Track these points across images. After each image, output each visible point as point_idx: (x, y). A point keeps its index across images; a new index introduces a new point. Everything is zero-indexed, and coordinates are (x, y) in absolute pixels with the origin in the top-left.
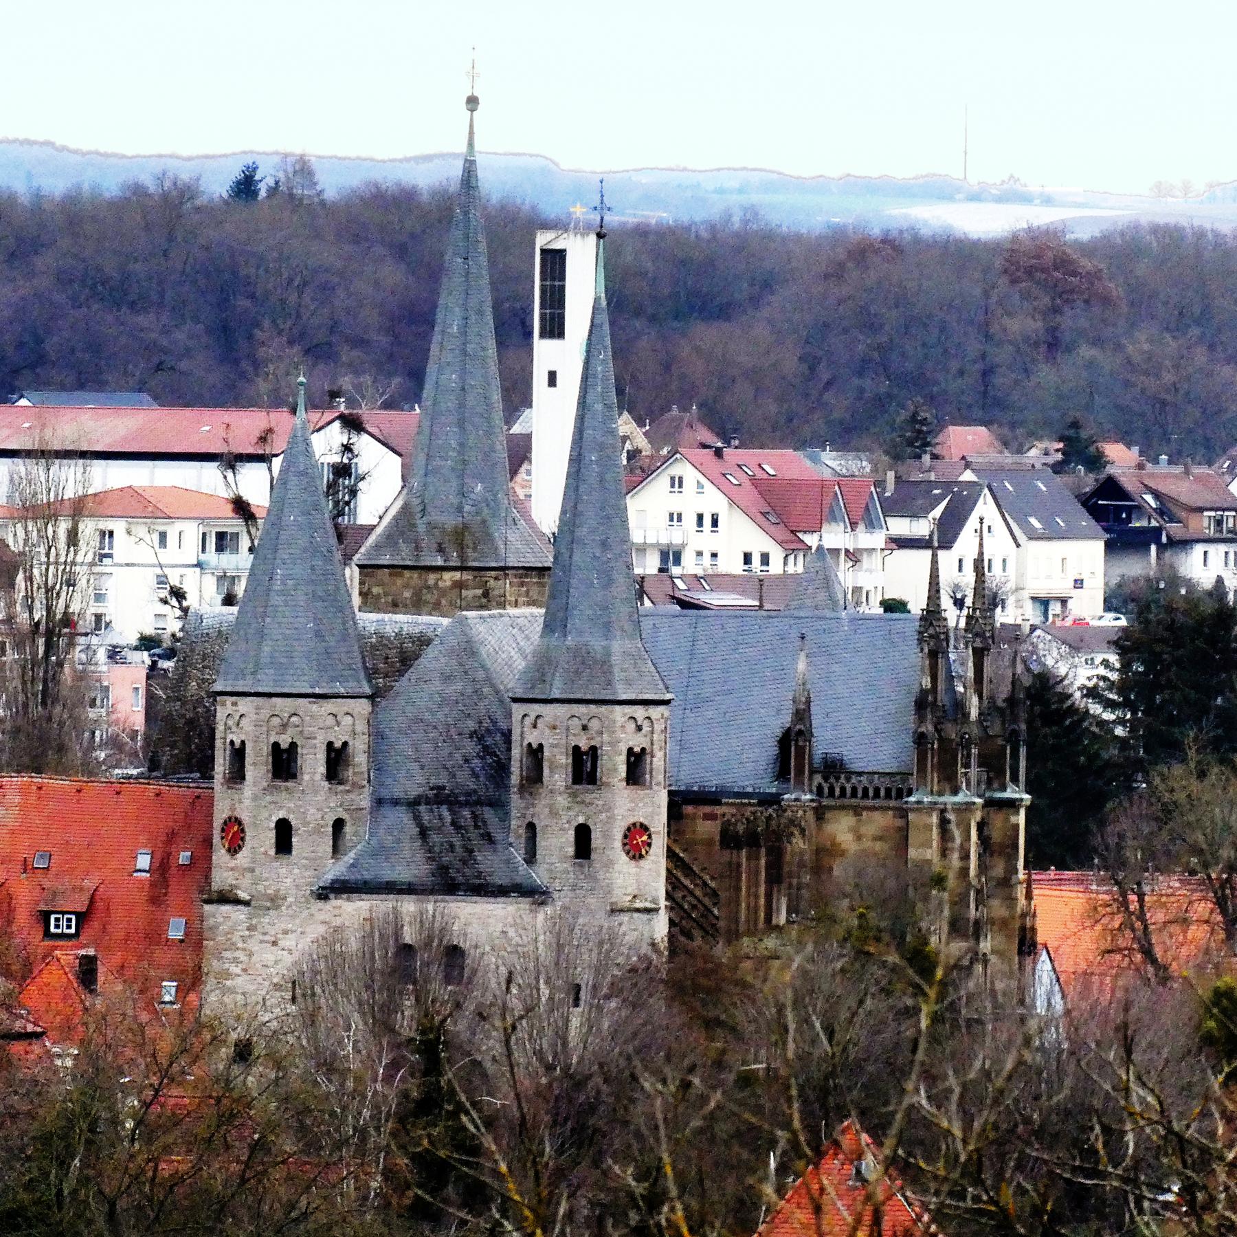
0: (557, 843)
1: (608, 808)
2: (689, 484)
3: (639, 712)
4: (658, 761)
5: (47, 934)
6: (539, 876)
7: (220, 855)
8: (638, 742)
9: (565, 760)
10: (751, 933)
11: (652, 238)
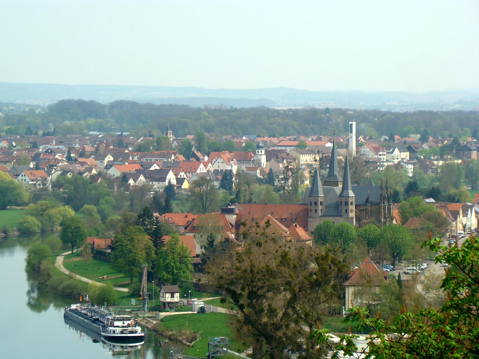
1: (349, 208)
3: (352, 198)
4: (354, 203)
6: (342, 214)
7: (309, 213)
8: (352, 201)
9: (344, 203)
10: (364, 219)
11: (167, 211)
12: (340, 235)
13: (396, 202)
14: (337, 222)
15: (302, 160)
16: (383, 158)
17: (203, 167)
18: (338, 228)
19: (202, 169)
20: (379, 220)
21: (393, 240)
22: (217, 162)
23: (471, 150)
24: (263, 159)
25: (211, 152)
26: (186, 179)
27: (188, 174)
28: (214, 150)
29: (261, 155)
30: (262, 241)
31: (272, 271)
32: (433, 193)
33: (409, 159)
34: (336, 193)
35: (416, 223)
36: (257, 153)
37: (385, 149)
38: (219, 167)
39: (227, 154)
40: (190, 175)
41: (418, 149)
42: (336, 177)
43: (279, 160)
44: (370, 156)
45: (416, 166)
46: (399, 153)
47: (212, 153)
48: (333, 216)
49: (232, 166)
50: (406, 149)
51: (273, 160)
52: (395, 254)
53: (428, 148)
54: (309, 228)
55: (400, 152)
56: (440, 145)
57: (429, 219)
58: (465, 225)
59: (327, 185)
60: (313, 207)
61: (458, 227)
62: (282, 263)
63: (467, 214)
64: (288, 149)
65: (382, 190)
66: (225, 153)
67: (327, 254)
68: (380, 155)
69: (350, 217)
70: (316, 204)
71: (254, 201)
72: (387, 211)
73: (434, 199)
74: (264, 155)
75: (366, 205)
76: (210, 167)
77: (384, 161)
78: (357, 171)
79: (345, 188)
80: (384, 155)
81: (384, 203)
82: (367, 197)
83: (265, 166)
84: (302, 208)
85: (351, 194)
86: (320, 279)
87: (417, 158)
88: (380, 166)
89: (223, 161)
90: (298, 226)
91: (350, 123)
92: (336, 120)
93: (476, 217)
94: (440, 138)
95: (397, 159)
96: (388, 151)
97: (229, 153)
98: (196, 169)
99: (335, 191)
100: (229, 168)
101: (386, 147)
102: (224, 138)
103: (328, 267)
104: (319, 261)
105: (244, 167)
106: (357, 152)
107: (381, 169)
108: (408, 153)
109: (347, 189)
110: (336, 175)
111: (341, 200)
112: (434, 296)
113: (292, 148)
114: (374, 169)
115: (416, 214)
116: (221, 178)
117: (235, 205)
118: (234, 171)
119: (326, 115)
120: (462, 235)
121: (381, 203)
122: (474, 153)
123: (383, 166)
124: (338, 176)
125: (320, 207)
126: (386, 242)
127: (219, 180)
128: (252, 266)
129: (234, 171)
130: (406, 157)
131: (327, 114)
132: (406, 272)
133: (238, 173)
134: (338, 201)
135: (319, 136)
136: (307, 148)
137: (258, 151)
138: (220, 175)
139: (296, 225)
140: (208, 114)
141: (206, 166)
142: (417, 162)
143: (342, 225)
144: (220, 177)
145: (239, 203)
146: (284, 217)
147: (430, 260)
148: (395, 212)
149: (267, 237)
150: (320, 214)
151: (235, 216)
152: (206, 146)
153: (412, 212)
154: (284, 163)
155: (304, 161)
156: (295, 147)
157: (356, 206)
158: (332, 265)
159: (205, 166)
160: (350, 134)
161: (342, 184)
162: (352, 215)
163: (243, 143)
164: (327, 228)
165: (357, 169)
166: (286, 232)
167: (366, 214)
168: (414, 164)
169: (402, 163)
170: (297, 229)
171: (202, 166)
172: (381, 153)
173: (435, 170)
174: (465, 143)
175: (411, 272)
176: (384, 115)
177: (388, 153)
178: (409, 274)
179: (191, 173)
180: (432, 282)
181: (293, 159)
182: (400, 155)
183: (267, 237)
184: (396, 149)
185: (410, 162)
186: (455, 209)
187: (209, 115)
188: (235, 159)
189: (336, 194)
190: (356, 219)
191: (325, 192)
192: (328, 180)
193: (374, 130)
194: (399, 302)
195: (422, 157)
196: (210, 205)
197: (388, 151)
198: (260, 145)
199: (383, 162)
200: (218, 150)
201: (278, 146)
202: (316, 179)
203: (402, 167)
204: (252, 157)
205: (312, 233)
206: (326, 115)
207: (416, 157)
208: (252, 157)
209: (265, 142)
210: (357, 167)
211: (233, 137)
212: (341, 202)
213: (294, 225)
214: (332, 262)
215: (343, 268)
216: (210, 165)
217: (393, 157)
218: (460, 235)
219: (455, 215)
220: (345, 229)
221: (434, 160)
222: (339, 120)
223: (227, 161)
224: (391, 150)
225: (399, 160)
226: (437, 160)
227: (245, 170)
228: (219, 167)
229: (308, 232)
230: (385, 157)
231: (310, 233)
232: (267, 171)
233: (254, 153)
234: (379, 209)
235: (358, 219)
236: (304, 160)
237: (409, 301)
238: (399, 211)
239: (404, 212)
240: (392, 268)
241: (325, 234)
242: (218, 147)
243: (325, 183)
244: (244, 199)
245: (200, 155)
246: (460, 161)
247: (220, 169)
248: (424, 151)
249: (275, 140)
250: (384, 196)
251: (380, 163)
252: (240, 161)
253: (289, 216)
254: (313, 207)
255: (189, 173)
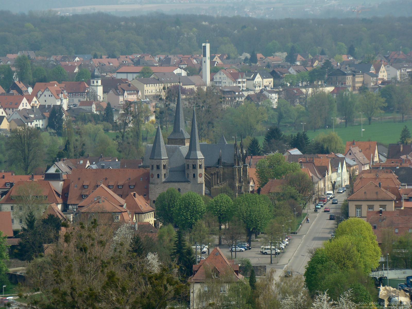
0: (191, 176)
2: (222, 74)
3: (200, 160)
4: (203, 166)
5: (119, 188)
6: (189, 180)
7: (151, 178)
9: (192, 166)
10: (215, 185)
12: (187, 207)
13: (254, 154)
14: (185, 190)
15: (147, 91)
16: (243, 86)
17: (27, 102)
18: (184, 199)
19: (25, 105)
20: (232, 186)
21: (249, 213)
22: (43, 96)
23: (345, 74)
24: (100, 90)
25: (35, 83)
26: (5, 118)
27: (7, 110)
28: (40, 79)
29: (97, 86)
30: (88, 245)
31: (96, 296)
32: (298, 142)
33: (273, 87)
34: (182, 154)
35: (276, 186)
36: (92, 84)
37: (244, 75)
38: (45, 101)
39: (56, 85)
40: (10, 112)
41: (284, 75)
42: (183, 133)
43: (118, 91)
44: (227, 84)
45: (281, 96)
46: (262, 80)
47: (37, 84)
48: (179, 182)
49: (62, 100)
50: (270, 75)
51: (111, 92)
52: (251, 230)
53: (295, 73)
54: (150, 196)
55: (263, 78)
56: (309, 69)
57: (291, 182)
58: (335, 182)
59: (172, 143)
60: (155, 172)
61: (326, 185)
62: (108, 285)
63: (337, 169)
64: (130, 77)
65: (236, 149)
66: (54, 84)
67: (162, 273)
68: (239, 82)
69: (199, 182)
70: (158, 167)
71: (86, 154)
72: (243, 174)
73: (300, 149)
74: (100, 86)
75: (218, 167)
76: (36, 102)
77: (244, 89)
78: (210, 110)
79: (192, 148)
80: (244, 82)
81: (238, 165)
82: (219, 157)
83: (102, 99)
84: (142, 171)
85: (200, 155)
86: (154, 303)
87: (283, 85)
88: (239, 96)
89: (51, 94)
90: (137, 195)
91: (203, 44)
92: (188, 34)
93: (347, 171)
94: (310, 56)
95: (259, 87)
96: (248, 78)
97: (57, 83)
98: (18, 104)
99: (180, 152)
100: (58, 103)
101: (245, 72)
102: (53, 58)
103: (162, 289)
104: (153, 281)
105: (76, 101)
106: (212, 79)
107: (240, 100)
108: (272, 79)
109: (195, 150)
110: (182, 131)
111: (188, 163)
112: (292, 302)
113: (135, 75)
114: (232, 100)
115: (277, 175)
116: (48, 116)
117: (64, 160)
118: (65, 107)
119: (176, 27)
120: (330, 196)
121: (235, 164)
122: (348, 78)
123: (243, 95)
124: (184, 132)
125: (163, 172)
126: (240, 216)
127: (47, 118)
128: (73, 289)
129: (65, 107)
130: (270, 84)
131: (178, 27)
132: (264, 252)
133: (69, 109)
134: (185, 164)
135: (168, 56)
136: (152, 76)
137: (93, 82)
138: (47, 111)
139: (134, 194)
140: (32, 27)
141: (29, 101)
142: (283, 90)
143: (188, 196)
144: (47, 114)
145: (69, 157)
146: (120, 183)
147: (292, 233)
148: (252, 172)
149: (93, 239)
150: (164, 180)
151: (62, 183)
152: (30, 74)
153: (272, 172)
154: (125, 95)
155: (149, 92)
156: (138, 74)
157: (205, 169)
158: (168, 285)
159: (28, 100)
160: (204, 59)
161: (189, 141)
162: (201, 180)
163: (75, 67)
164: (172, 197)
165: (211, 108)
166: (122, 206)
167: (217, 178)
168: (279, 93)
169: (265, 92)
170: (136, 199)
171: (25, 100)
172: (240, 80)
173: (304, 100)
174: (339, 64)
175: (268, 252)
176: (244, 27)
177: (248, 80)
178: (267, 254)
179: (11, 110)
180: (289, 284)
181: (136, 90)
182: (262, 82)
183: (93, 239)
184: (258, 75)
185: (274, 90)
186: (323, 165)
187: (35, 27)
188: (65, 91)
189: (181, 155)
190: (205, 185)
191: (170, 153)
192: (173, 137)
193: (233, 45)
194: (251, 306)
195: (289, 85)
196: (33, 159)
197: (248, 78)
198: (95, 74)
199: (243, 90)
200: (44, 80)
201: (117, 73)
202: (158, 138)
203: (265, 97)
204: (85, 88)
205: (154, 202)
206: (176, 27)
207: (282, 83)
208: (85, 88)
209: (102, 67)
210: (208, 106)
211: (64, 59)
212: (188, 165)
213: (132, 193)
214: (168, 282)
215: (180, 289)
216: (35, 99)
217: (254, 84)
218: (328, 196)
219: (323, 171)
220: (192, 201)
221: (302, 87)
222: (192, 33)
223: (55, 93)
224: (252, 76)
225: (261, 88)
226: (306, 87)
227: (78, 104)
228: (45, 101)
229: (149, 201)
230: (245, 85)
231: (152, 202)
232: (105, 106)
233: (89, 84)
234: (233, 171)
235: (208, 184)
236: (149, 91)
237: (263, 304)
238: (257, 171)
239: (263, 172)
240: (247, 247)
241: (169, 205)
242: (45, 76)
243: (170, 141)
244: (75, 151)
245: (22, 87)
246: (330, 89)
247: (47, 104)
248: (291, 76)
249: (114, 63)
250: (239, 156)
251: (239, 92)
252: (72, 92)
253: (127, 182)
254: (155, 172)
255: (9, 110)
